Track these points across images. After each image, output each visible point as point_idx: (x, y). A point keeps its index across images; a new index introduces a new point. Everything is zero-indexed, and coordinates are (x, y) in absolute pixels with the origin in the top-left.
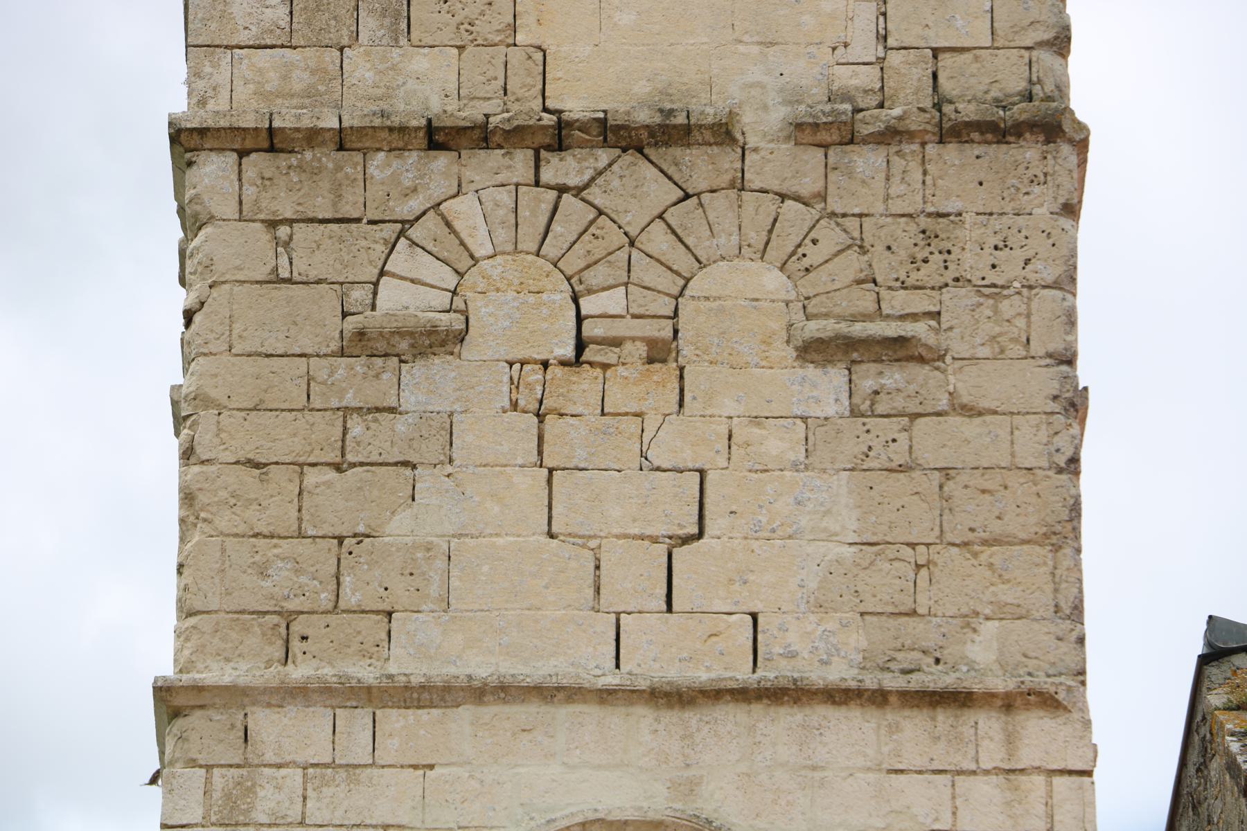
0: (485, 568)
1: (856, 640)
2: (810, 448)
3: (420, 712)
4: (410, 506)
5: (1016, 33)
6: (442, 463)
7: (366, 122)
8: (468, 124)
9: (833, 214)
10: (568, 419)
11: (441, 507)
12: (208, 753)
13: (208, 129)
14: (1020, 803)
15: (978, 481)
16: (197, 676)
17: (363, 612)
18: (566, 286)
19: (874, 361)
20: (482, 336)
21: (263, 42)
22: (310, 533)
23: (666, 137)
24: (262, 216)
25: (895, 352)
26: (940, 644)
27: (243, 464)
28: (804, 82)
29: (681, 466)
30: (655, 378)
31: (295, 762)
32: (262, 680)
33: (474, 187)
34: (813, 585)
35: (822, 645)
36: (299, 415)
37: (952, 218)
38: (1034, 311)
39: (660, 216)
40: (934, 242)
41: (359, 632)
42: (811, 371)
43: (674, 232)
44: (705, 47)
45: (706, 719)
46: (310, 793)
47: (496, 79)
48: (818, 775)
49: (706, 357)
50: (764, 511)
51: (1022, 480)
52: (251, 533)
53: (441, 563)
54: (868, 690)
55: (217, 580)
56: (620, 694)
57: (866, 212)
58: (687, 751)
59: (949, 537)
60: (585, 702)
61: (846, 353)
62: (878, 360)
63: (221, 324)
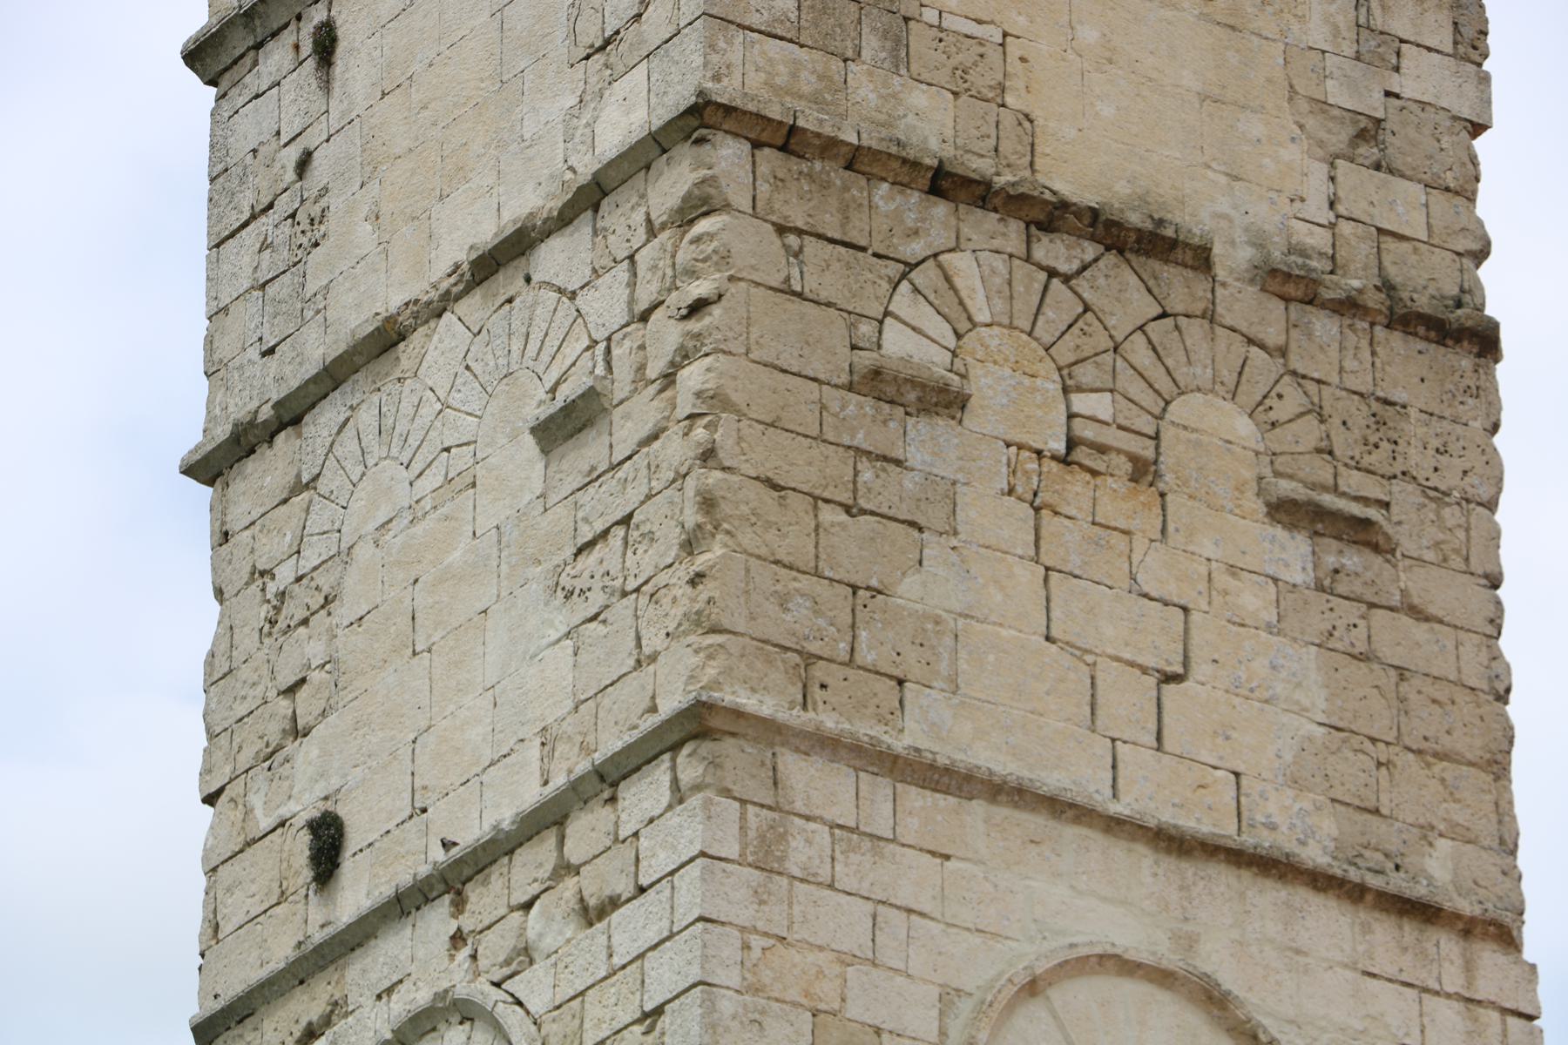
0: (991, 658)
1: (1328, 825)
2: (1282, 613)
3: (938, 795)
4: (919, 572)
5: (1449, 234)
6: (946, 533)
7: (882, 147)
8: (977, 177)
9: (1294, 373)
10: (1063, 519)
11: (948, 580)
12: (743, 787)
13: (735, 109)
14: (1480, 1036)
15: (1431, 690)
16: (738, 700)
17: (877, 673)
18: (1056, 377)
19: (1335, 538)
20: (982, 407)
21: (774, 31)
22: (827, 573)
23: (1150, 247)
24: (774, 218)
25: (1356, 533)
26: (1402, 850)
27: (762, 481)
28: (1266, 227)
29: (1167, 598)
30: (1142, 498)
31: (822, 819)
32: (798, 721)
33: (971, 246)
34: (1288, 757)
35: (1299, 823)
36: (814, 444)
37: (1398, 408)
38: (1472, 526)
39: (1141, 328)
40: (1383, 428)
41: (875, 694)
42: (1279, 532)
43: (1154, 349)
44: (1178, 163)
45: (1202, 874)
46: (838, 855)
47: (989, 137)
48: (1301, 959)
49: (1185, 490)
50: (1243, 668)
51: (1467, 699)
52: (772, 559)
53: (948, 640)
54: (1350, 882)
55: (742, 600)
56: (1127, 827)
57: (1324, 379)
58: (1185, 904)
59: (1408, 741)
60: (1090, 826)
61: (1313, 521)
62: (1339, 538)
63: (739, 323)
